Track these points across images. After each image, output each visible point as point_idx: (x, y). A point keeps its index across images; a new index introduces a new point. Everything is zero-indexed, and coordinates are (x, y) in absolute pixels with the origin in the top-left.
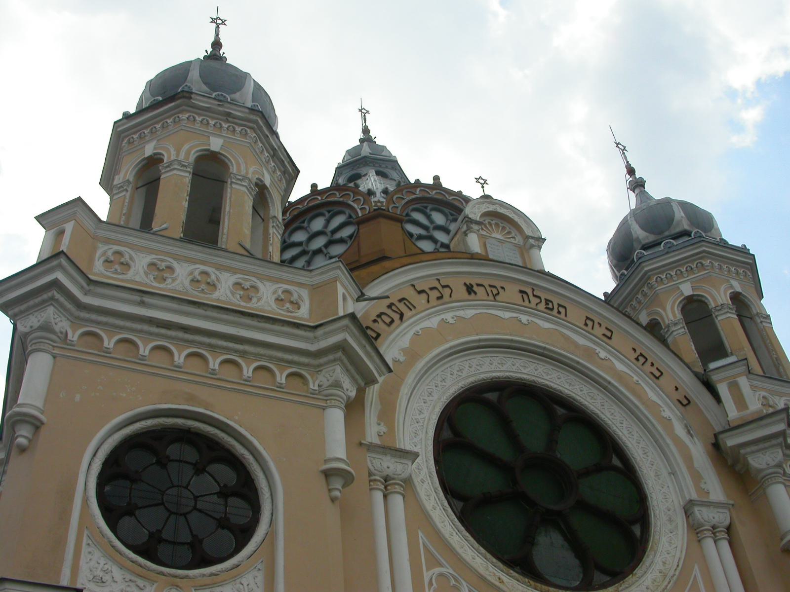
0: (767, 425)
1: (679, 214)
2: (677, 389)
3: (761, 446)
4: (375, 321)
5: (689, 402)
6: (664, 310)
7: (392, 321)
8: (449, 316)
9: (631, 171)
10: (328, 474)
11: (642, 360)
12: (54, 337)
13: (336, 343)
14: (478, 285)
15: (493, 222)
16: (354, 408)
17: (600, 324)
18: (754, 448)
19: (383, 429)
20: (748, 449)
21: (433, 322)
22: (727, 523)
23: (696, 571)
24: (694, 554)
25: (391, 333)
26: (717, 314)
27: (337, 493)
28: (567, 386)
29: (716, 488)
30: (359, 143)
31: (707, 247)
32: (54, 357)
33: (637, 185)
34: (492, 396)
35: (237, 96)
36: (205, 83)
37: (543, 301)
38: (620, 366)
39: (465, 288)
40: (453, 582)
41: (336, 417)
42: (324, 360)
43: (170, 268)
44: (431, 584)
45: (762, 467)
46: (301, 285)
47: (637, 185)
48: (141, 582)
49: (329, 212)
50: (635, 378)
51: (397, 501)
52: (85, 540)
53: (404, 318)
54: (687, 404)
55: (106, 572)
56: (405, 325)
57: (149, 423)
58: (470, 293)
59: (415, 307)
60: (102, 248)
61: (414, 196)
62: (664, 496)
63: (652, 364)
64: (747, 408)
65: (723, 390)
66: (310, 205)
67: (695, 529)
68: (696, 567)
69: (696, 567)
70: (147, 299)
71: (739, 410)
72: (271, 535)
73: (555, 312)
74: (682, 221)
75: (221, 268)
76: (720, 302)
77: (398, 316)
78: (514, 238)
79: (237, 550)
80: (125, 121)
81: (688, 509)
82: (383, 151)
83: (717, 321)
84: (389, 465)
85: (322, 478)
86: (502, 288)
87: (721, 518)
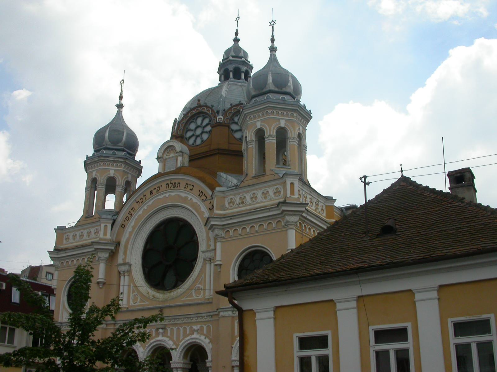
1: (291, 84)
4: (125, 221)
9: (237, 34)
13: (118, 252)
21: (140, 212)
25: (129, 222)
26: (290, 140)
27: (101, 286)
30: (20, 273)
33: (236, 40)
35: (104, 143)
43: (245, 197)
44: (132, 298)
47: (236, 40)
49: (203, 116)
50: (136, 217)
51: (126, 277)
64: (294, 195)
71: (291, 194)
73: (176, 188)
74: (290, 88)
76: (293, 136)
83: (289, 144)
85: (97, 284)
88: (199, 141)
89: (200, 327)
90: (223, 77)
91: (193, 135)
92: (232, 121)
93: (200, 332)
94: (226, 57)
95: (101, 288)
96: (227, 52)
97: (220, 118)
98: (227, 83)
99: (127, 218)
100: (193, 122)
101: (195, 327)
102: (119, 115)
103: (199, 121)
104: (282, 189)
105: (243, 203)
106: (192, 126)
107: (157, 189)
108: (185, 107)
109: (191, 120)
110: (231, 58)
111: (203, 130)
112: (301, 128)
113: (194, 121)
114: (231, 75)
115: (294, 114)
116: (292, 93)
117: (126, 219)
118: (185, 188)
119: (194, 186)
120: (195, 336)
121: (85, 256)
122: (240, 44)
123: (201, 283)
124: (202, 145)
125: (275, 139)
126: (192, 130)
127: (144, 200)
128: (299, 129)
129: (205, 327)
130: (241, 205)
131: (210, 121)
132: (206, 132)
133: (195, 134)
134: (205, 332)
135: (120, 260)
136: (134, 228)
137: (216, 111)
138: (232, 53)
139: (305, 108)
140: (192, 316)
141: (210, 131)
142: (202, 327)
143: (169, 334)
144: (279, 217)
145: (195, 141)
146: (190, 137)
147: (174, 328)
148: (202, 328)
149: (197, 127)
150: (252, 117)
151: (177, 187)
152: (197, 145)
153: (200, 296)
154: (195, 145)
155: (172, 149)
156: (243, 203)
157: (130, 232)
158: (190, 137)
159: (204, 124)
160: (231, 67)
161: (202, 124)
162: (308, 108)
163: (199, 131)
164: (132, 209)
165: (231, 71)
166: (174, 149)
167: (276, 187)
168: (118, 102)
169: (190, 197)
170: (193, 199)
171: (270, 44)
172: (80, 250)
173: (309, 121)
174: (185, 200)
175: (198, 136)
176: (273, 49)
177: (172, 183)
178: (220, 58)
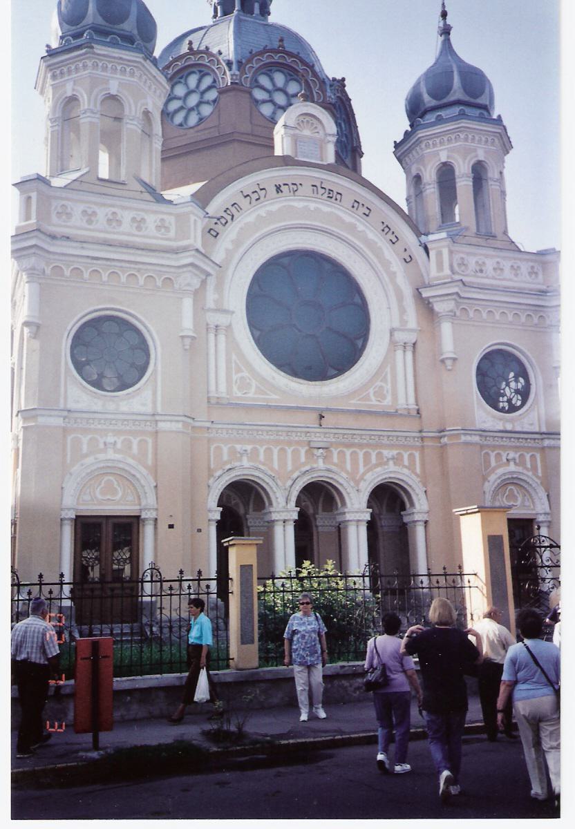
0: (448, 287)
2: (406, 250)
3: (442, 298)
4: (216, 223)
7: (227, 222)
10: (182, 337)
11: (387, 230)
14: (285, 184)
16: (198, 295)
17: (363, 205)
18: (438, 299)
19: (216, 296)
20: (435, 299)
22: (414, 341)
23: (234, 357)
24: (389, 359)
29: (412, 318)
32: (40, 284)
34: (285, 261)
37: (327, 191)
38: (371, 236)
39: (275, 188)
40: (248, 381)
41: (188, 303)
42: (181, 270)
44: (236, 382)
45: (440, 311)
46: (170, 214)
48: (96, 400)
51: (222, 338)
53: (234, 219)
56: (234, 223)
59: (241, 209)
62: (382, 316)
63: (393, 233)
65: (432, 253)
66: (186, 64)
67: (393, 344)
70: (85, 245)
72: (155, 371)
73: (333, 200)
75: (124, 208)
77: (230, 217)
79: (139, 379)
80: (48, 58)
81: (392, 332)
84: (222, 320)
86: (301, 184)
87: (412, 338)
89: (397, 454)
91: (182, 108)
92: (256, 84)
95: (449, 370)
99: (223, 221)
100: (180, 82)
101: (387, 453)
103: (193, 80)
105: (481, 271)
109: (263, 71)
113: (182, 80)
115: (136, 72)
116: (122, 25)
118: (353, 207)
121: (139, 270)
123: (239, 370)
124: (199, 128)
126: (179, 98)
130: (479, 274)
131: (215, 81)
132: (208, 103)
133: (184, 106)
134: (406, 462)
135: (211, 297)
136: (237, 243)
140: (299, 429)
141: (214, 101)
142: (522, 456)
143: (335, 460)
144: (479, 305)
145: (186, 118)
147: (525, 454)
150: (65, 69)
152: (191, 128)
153: (387, 400)
154: (185, 127)
156: (481, 271)
157: (227, 250)
158: (176, 111)
159: (204, 86)
163: (193, 100)
164: (233, 205)
169: (361, 227)
170: (368, 232)
174: (352, 228)
175: (192, 109)
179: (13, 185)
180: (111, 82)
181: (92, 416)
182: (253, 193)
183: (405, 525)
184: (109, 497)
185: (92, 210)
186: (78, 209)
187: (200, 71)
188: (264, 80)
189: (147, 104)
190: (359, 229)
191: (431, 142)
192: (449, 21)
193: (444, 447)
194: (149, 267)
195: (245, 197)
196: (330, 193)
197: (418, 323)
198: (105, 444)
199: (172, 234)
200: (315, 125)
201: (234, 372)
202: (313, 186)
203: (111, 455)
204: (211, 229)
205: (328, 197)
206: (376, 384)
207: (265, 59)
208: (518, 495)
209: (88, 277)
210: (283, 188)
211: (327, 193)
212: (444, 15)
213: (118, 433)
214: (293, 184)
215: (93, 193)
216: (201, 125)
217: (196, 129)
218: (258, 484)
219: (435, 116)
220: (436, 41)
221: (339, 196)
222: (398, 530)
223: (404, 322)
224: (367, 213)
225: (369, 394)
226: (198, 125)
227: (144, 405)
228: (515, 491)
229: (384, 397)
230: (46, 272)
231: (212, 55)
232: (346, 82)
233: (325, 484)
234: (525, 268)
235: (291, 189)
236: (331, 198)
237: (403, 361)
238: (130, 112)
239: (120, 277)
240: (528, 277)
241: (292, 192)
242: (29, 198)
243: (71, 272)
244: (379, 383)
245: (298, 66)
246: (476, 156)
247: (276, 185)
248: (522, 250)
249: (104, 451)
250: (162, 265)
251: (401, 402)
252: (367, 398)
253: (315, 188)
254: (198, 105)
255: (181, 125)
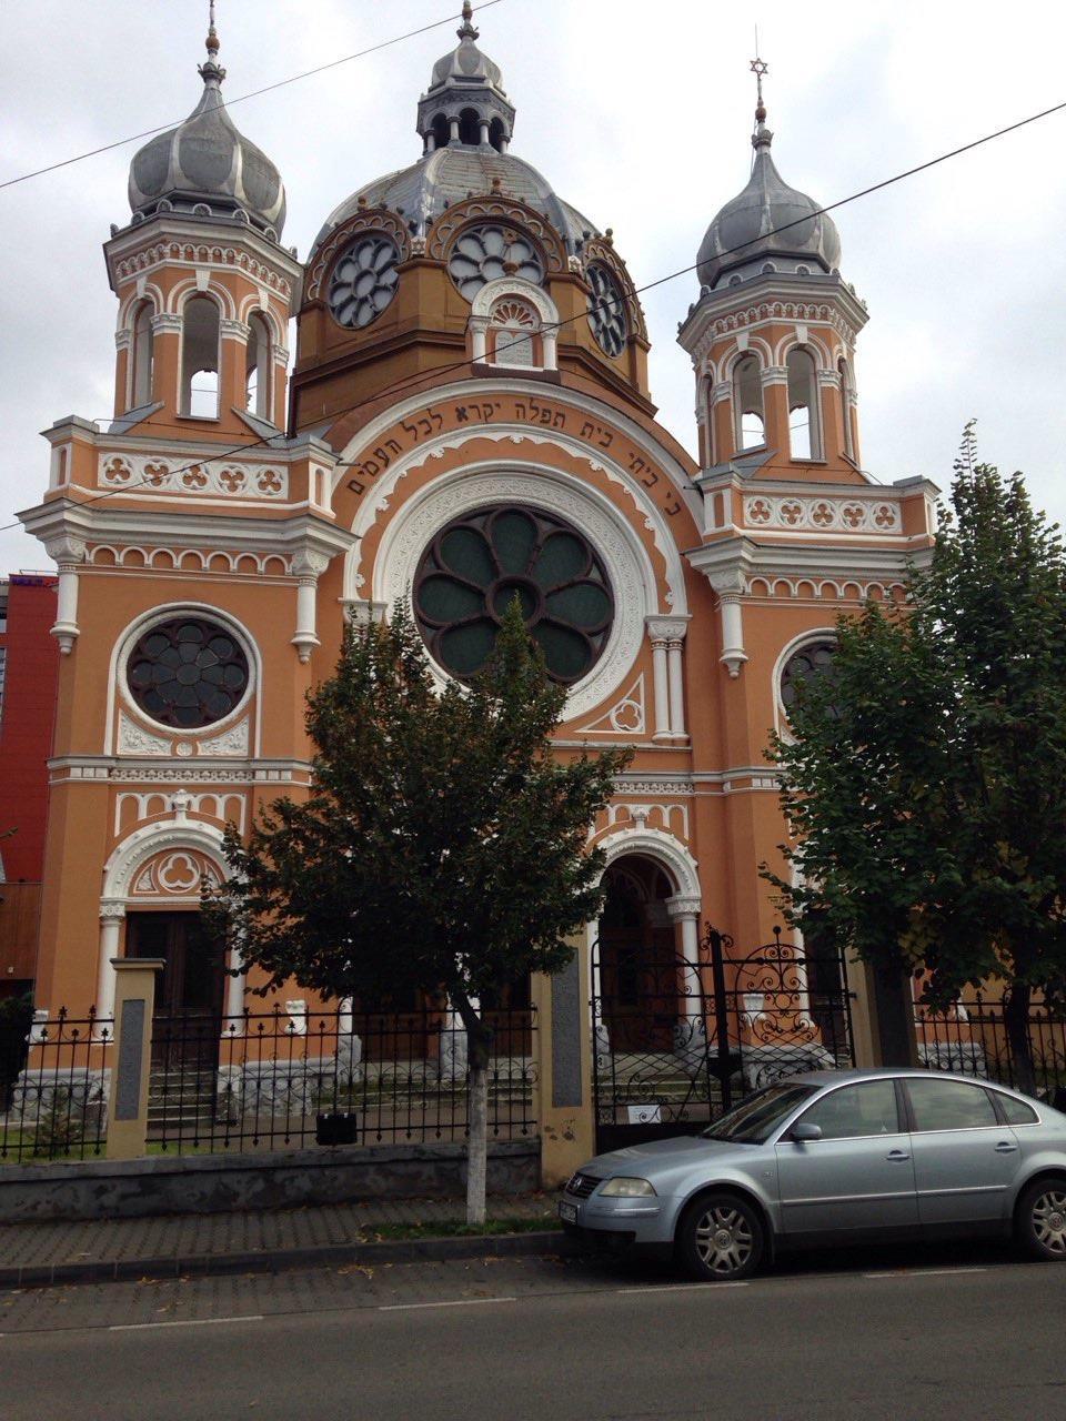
2: (669, 496)
3: (721, 567)
4: (361, 473)
5: (679, 509)
6: (717, 365)
8: (437, 452)
11: (638, 465)
12: (75, 559)
15: (509, 306)
18: (716, 569)
20: (711, 569)
22: (682, 634)
24: (644, 662)
28: (556, 501)
29: (679, 604)
31: (773, 286)
33: (467, 34)
36: (187, 177)
37: (541, 412)
39: (456, 414)
47: (467, 34)
49: (376, 242)
52: (120, 717)
54: (676, 512)
55: (137, 738)
57: (160, 618)
58: (460, 420)
60: (103, 457)
61: (465, 220)
63: (649, 470)
68: (642, 675)
69: (642, 675)
78: (531, 322)
82: (477, 65)
86: (498, 405)
88: (365, 316)
90: (431, 140)
91: (351, 299)
93: (653, 821)
94: (438, 81)
96: (443, 67)
97: (418, 243)
98: (442, 151)
102: (763, 168)
103: (365, 257)
104: (899, 513)
106: (348, 274)
107: (481, 409)
108: (326, 226)
110: (451, 82)
111: (378, 282)
112: (844, 346)
113: (353, 257)
114: (455, 131)
117: (365, 466)
119: (659, 482)
120: (641, 830)
122: (479, 44)
125: (245, 336)
126: (348, 285)
127: (435, 429)
128: (841, 351)
129: (666, 811)
131: (395, 255)
132: (385, 288)
134: (667, 823)
137: (407, 225)
138: (457, 69)
139: (854, 294)
141: (395, 285)
145: (356, 314)
146: (343, 306)
148: (656, 813)
149: (360, 277)
151: (555, 424)
152: (363, 328)
153: (637, 728)
155: (514, 307)
157: (379, 512)
158: (343, 306)
159: (380, 264)
160: (452, 111)
161: (373, 265)
162: (860, 296)
163: (365, 287)
164: (387, 444)
165: (453, 119)
166: (528, 315)
167: (882, 504)
168: (203, 57)
169: (596, 465)
171: (203, 57)
172: (640, 553)
173: (861, 327)
175: (364, 301)
176: (762, 141)
177: (536, 409)
178: (423, 83)
179: (41, 434)
180: (198, 273)
181: (155, 765)
182: (420, 423)
183: (671, 918)
184: (179, 883)
185: (161, 463)
186: (137, 466)
187: (534, 257)
188: (469, 248)
189: (258, 301)
190: (594, 467)
191: (735, 319)
192: (768, 125)
193: (725, 799)
194: (217, 542)
195: (408, 430)
196: (544, 416)
197: (690, 608)
198: (173, 806)
199: (283, 493)
200: (526, 312)
201: (628, 695)
202: (517, 405)
203: (182, 822)
204: (353, 482)
205: (543, 421)
206: (622, 702)
207: (470, 213)
208: (194, 870)
209: (235, 568)
210: (469, 413)
211: (540, 415)
212: (761, 116)
213: (192, 789)
214: (484, 405)
215: (659, 443)
216: (376, 323)
217: (370, 329)
218: (661, 862)
219: (729, 280)
220: (748, 155)
221: (560, 420)
222: (675, 921)
223: (665, 607)
224: (606, 442)
225: (608, 717)
226: (372, 323)
227: (235, 747)
228: (189, 862)
229: (634, 724)
230: (87, 558)
231: (391, 216)
232: (614, 237)
233: (656, 863)
234: (870, 512)
235: (482, 414)
236: (547, 422)
237: (668, 671)
238: (228, 316)
239: (256, 564)
240: (876, 526)
241: (483, 417)
242: (64, 453)
243: (211, 563)
244: (625, 701)
245: (523, 219)
246: (795, 338)
247: (457, 410)
248: (875, 482)
249: (172, 816)
250: (207, 537)
251: (663, 732)
252: (607, 724)
253: (521, 410)
254: (373, 293)
255: (350, 324)
